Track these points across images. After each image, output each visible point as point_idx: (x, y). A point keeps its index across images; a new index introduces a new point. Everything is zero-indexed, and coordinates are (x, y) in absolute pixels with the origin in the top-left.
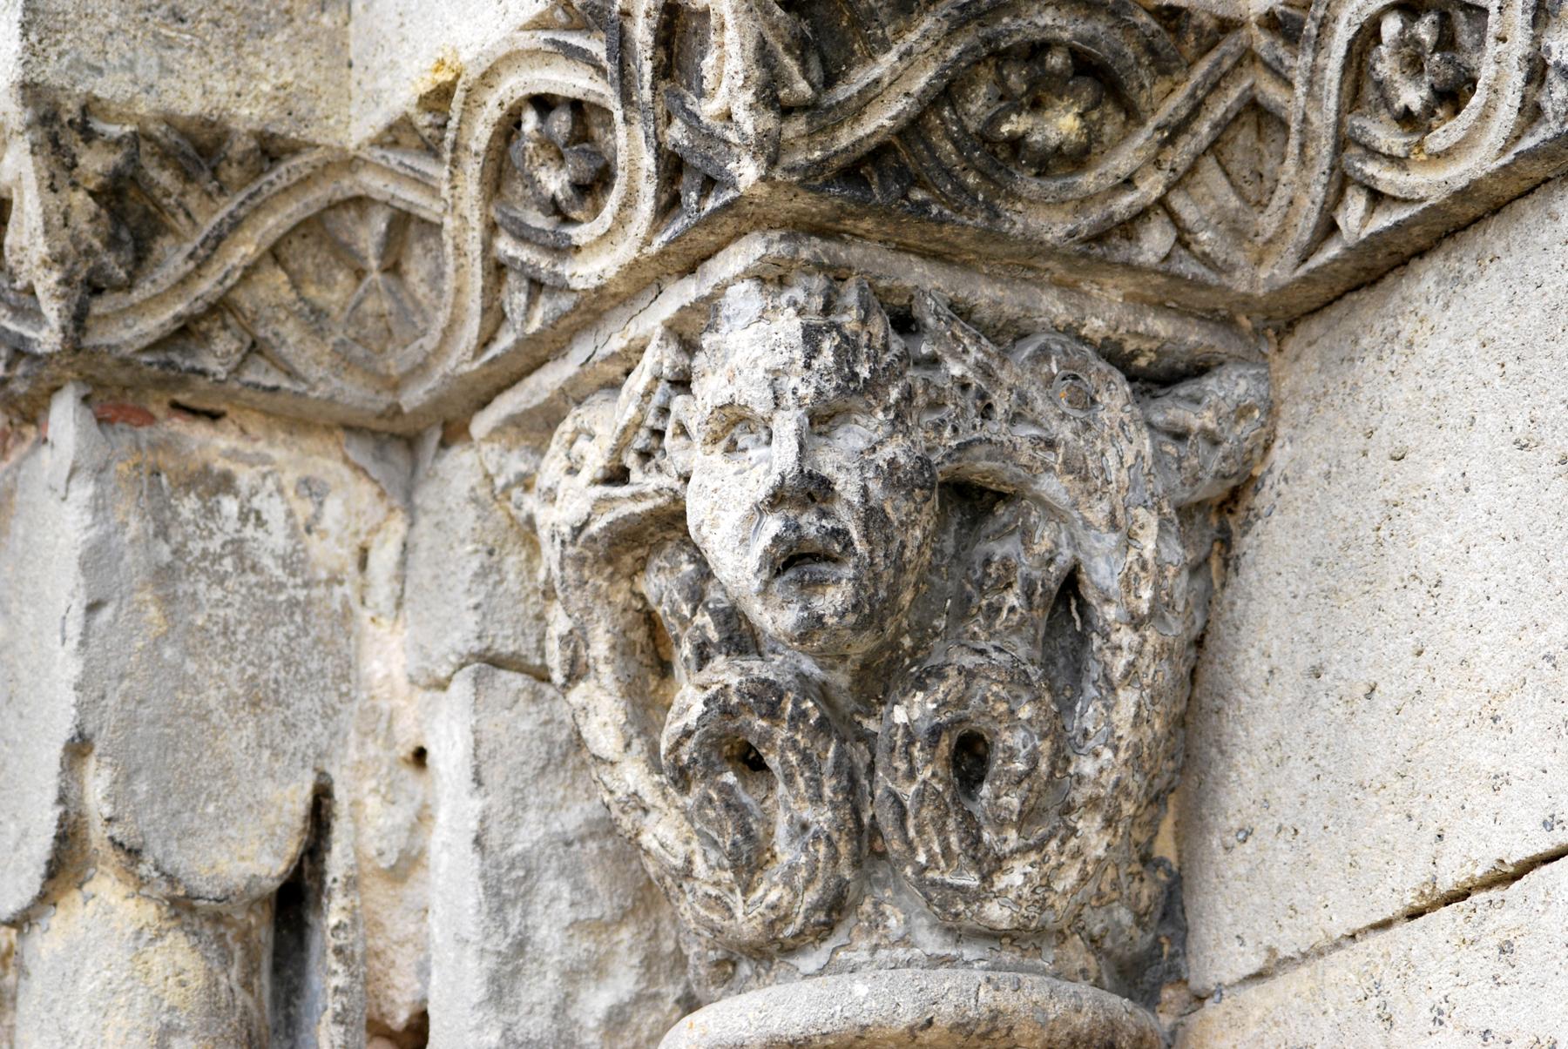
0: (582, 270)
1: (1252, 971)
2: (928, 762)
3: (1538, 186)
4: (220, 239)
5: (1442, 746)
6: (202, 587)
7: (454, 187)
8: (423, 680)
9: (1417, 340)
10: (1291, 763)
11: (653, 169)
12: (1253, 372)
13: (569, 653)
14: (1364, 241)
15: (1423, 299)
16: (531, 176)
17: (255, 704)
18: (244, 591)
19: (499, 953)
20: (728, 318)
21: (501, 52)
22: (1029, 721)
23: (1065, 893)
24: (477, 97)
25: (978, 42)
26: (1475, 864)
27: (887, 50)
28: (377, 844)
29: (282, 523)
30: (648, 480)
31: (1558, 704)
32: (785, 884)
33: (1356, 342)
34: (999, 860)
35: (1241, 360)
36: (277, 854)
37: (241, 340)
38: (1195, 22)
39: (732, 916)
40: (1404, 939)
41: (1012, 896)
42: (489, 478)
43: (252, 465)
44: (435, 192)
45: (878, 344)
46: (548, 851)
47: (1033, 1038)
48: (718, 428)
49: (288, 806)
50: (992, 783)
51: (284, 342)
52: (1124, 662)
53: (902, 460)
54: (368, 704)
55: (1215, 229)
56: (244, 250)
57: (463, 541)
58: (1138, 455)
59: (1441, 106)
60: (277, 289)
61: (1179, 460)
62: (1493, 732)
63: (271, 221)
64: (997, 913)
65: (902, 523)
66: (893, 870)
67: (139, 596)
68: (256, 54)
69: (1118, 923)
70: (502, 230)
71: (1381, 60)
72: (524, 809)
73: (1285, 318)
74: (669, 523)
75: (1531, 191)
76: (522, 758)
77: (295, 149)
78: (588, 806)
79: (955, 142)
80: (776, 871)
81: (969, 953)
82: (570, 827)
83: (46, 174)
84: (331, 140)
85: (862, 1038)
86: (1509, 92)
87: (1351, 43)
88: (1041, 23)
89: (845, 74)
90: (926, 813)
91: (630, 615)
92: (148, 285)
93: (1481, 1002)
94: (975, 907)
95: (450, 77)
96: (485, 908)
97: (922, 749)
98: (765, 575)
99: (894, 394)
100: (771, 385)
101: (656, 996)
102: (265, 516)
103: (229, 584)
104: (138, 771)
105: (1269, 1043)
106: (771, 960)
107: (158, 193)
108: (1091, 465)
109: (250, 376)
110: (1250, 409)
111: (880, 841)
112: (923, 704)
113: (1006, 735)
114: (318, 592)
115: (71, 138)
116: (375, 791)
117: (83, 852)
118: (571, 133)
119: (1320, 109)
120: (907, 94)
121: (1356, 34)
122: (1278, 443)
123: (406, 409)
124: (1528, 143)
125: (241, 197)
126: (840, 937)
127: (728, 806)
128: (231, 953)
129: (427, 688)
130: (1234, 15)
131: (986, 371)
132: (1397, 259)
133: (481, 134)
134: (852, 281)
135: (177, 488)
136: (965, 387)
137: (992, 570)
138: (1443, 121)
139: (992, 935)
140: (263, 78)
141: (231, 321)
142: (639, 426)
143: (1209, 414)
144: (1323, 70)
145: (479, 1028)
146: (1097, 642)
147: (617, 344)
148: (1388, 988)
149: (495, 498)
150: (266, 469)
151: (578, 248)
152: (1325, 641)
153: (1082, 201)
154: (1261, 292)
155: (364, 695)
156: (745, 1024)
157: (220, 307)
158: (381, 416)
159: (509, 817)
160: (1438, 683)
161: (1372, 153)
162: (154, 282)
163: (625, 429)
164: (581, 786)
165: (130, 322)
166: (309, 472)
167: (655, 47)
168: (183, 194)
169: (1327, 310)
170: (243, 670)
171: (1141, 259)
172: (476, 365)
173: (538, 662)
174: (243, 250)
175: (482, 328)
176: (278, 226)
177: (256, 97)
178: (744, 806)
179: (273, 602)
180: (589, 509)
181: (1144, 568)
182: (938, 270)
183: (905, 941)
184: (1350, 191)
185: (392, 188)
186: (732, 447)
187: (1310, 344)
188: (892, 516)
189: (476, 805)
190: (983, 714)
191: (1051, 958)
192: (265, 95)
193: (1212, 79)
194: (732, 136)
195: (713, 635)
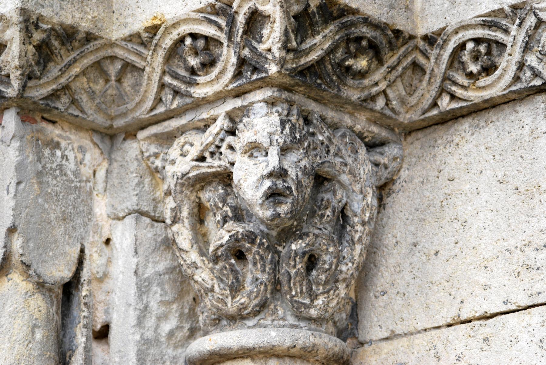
0: (198, 91)
1: (384, 337)
2: (300, 263)
3: (510, 101)
4: (70, 65)
5: (464, 273)
6: (50, 179)
7: (152, 58)
8: (112, 216)
9: (460, 144)
10: (404, 272)
11: (235, 63)
12: (398, 146)
13: (174, 214)
14: (447, 111)
15: (463, 131)
16: (185, 59)
17: (64, 220)
18: (62, 182)
19: (140, 309)
20: (254, 114)
21: (183, 18)
22: (332, 252)
23: (332, 308)
24: (169, 31)
25: (344, 35)
26: (476, 312)
27: (319, 34)
28: (96, 269)
29: (73, 160)
30: (214, 162)
31: (511, 265)
32: (248, 297)
33: (436, 141)
34: (317, 295)
35: (395, 142)
36: (69, 270)
37: (69, 99)
38: (403, 35)
39: (227, 305)
40: (446, 333)
41: (318, 307)
42: (142, 152)
43: (65, 140)
44: (145, 59)
45: (301, 128)
46: (155, 277)
47: (323, 353)
48: (247, 149)
49: (73, 255)
50: (317, 271)
51: (82, 101)
52: (358, 236)
53: (308, 166)
54: (96, 223)
55: (397, 101)
56: (76, 70)
57: (132, 173)
58: (368, 170)
59: (484, 72)
60: (83, 83)
61: (376, 172)
62: (485, 271)
63: (85, 61)
64: (313, 312)
65: (306, 186)
66: (282, 296)
67: (32, 181)
68: (87, 5)
69: (342, 318)
70: (167, 74)
71: (465, 55)
72: (148, 263)
73: (410, 131)
74: (225, 178)
75: (508, 102)
76: (148, 246)
77: (96, 38)
78: (165, 263)
79: (332, 66)
80: (245, 293)
81: (302, 324)
82: (161, 270)
83: (23, 39)
84: (107, 37)
85: (272, 349)
86: (510, 72)
87: (454, 48)
88: (363, 31)
89: (305, 41)
90: (297, 279)
91: (195, 204)
92: (46, 78)
93: (475, 355)
94: (307, 310)
95: (159, 23)
96: (137, 295)
97: (299, 258)
98: (263, 199)
99: (306, 144)
100: (269, 137)
101: (182, 327)
102: (69, 158)
103: (58, 179)
104: (30, 239)
105: (390, 361)
106: (236, 321)
107: (53, 48)
108: (356, 172)
109: (70, 111)
110: (397, 158)
111: (279, 286)
112: (301, 244)
113: (324, 256)
114: (83, 184)
115: (32, 28)
116: (96, 252)
117: (10, 264)
118: (204, 47)
119: (438, 68)
120: (322, 49)
121: (456, 46)
122: (403, 170)
123: (115, 127)
124: (514, 88)
125: (78, 53)
126: (262, 315)
127: (232, 270)
128: (54, 302)
129: (114, 219)
130: (414, 35)
131: (330, 140)
132: (454, 117)
133: (168, 42)
134: (295, 106)
135: (43, 146)
136: (322, 144)
137: (324, 203)
138: (483, 77)
139: (310, 319)
140: (89, 14)
141: (67, 92)
142: (212, 144)
143: (386, 159)
144: (442, 55)
145: (133, 334)
146: (349, 228)
147: (205, 116)
148: (439, 348)
149: (143, 159)
150: (69, 142)
151: (198, 84)
152: (419, 235)
153: (363, 88)
154: (406, 122)
155: (95, 220)
156: (232, 341)
157: (66, 88)
158: (105, 128)
159: (145, 265)
160: (464, 253)
161: (455, 83)
162: (48, 77)
163: (207, 144)
164: (163, 256)
165: (38, 90)
166: (82, 144)
167: (245, 25)
168: (60, 49)
169: (425, 130)
170: (61, 208)
171: (376, 108)
172: (147, 116)
173: (153, 214)
174: (76, 69)
175: (152, 105)
176: (87, 63)
177: (87, 20)
178: (237, 271)
179: (70, 186)
180: (189, 168)
181: (368, 207)
182: (318, 105)
183: (283, 319)
184: (444, 94)
185: (126, 55)
186: (251, 156)
187: (417, 140)
188: (303, 184)
189: (135, 260)
190: (319, 249)
191: (324, 328)
192: (89, 19)
193: (405, 54)
194: (269, 56)
195: (230, 214)
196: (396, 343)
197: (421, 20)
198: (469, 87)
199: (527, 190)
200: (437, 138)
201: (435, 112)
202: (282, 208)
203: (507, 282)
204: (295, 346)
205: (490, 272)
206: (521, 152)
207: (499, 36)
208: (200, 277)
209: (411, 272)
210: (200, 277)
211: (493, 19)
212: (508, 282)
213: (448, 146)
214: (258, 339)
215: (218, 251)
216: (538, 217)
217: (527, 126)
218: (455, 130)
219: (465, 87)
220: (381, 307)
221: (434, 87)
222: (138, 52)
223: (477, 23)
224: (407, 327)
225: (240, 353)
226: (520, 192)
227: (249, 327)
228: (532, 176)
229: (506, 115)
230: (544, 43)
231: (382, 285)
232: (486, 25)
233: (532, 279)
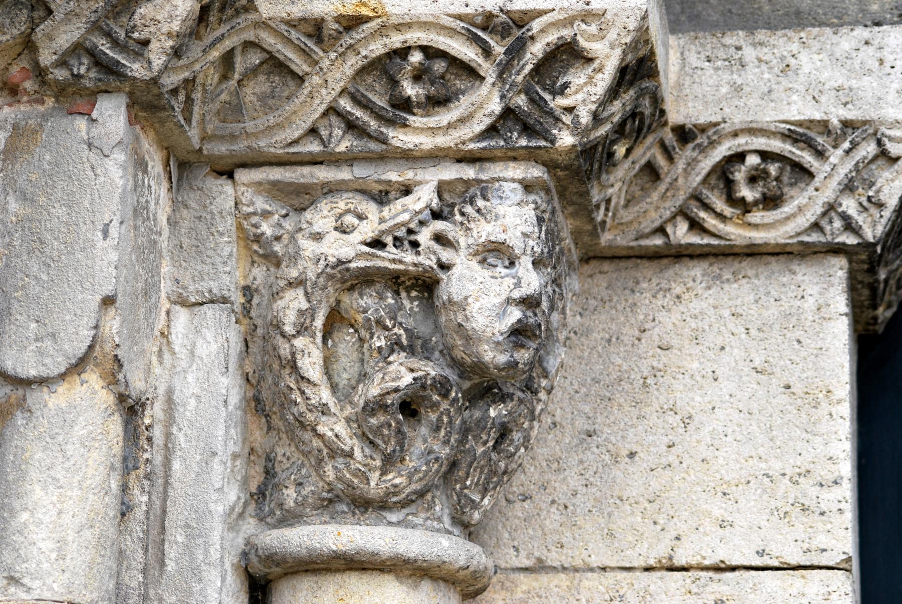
1: (523, 566)
5: (685, 496)
10: (566, 473)
21: (423, 19)
33: (638, 283)
39: (368, 484)
71: (740, 171)
123: (205, 152)
124: (806, 239)
125: (228, 28)
126: (412, 508)
133: (377, 48)
147: (393, 176)
148: (629, 600)
160: (684, 465)
161: (707, 207)
172: (282, 151)
183: (439, 520)
187: (600, 272)
194: (567, 119)
196: (545, 578)
197: (676, 100)
198: (731, 219)
199: (807, 393)
200: (641, 279)
201: (658, 241)
202: (520, 354)
203: (763, 523)
204: (468, 567)
205: (733, 502)
206: (799, 334)
207: (807, 158)
208: (332, 430)
209: (582, 475)
210: (332, 430)
211: (806, 131)
212: (766, 524)
213: (660, 295)
214: (424, 547)
215: (387, 396)
216: (825, 437)
217: (810, 298)
218: (676, 274)
219: (725, 217)
220: (519, 518)
221: (668, 204)
222: (307, 49)
223: (778, 130)
224: (570, 559)
225: (388, 563)
226: (794, 394)
227: (390, 523)
228: (816, 374)
229: (773, 273)
230: (881, 187)
231: (522, 485)
232: (791, 137)
233: (811, 527)
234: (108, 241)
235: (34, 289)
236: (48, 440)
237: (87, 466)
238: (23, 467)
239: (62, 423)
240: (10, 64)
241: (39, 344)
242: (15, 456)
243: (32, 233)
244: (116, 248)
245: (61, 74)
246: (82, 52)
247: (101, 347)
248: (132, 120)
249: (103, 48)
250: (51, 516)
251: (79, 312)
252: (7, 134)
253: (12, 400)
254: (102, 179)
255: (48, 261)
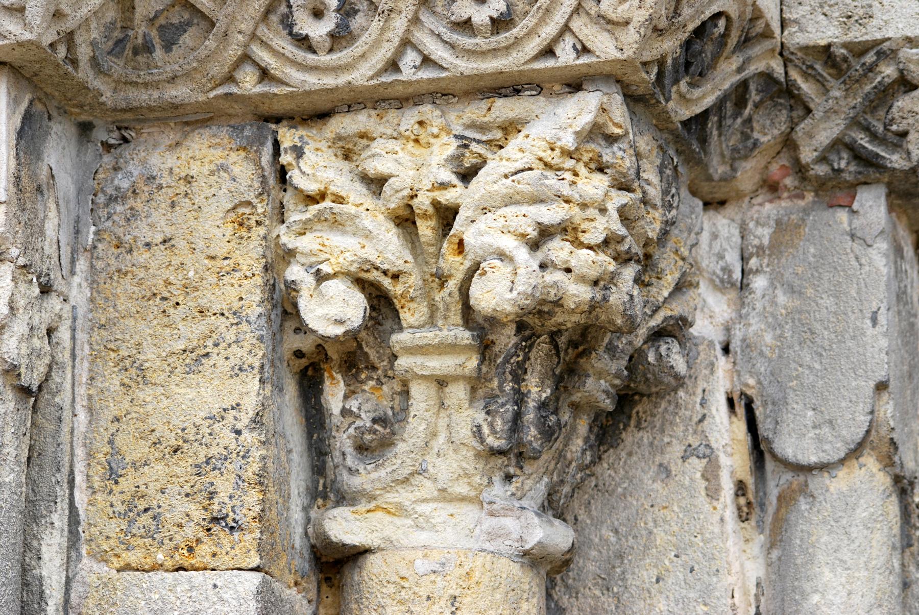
124: (383, 79)
234: (877, 328)
235: (808, 379)
236: (832, 523)
237: (871, 547)
238: (810, 550)
239: (844, 507)
240: (769, 163)
241: (817, 431)
242: (802, 540)
243: (803, 324)
244: (885, 335)
245: (821, 170)
246: (841, 147)
247: (877, 431)
248: (891, 209)
249: (862, 142)
250: (841, 597)
251: (854, 399)
252: (771, 230)
253: (794, 486)
254: (867, 268)
255: (820, 350)
